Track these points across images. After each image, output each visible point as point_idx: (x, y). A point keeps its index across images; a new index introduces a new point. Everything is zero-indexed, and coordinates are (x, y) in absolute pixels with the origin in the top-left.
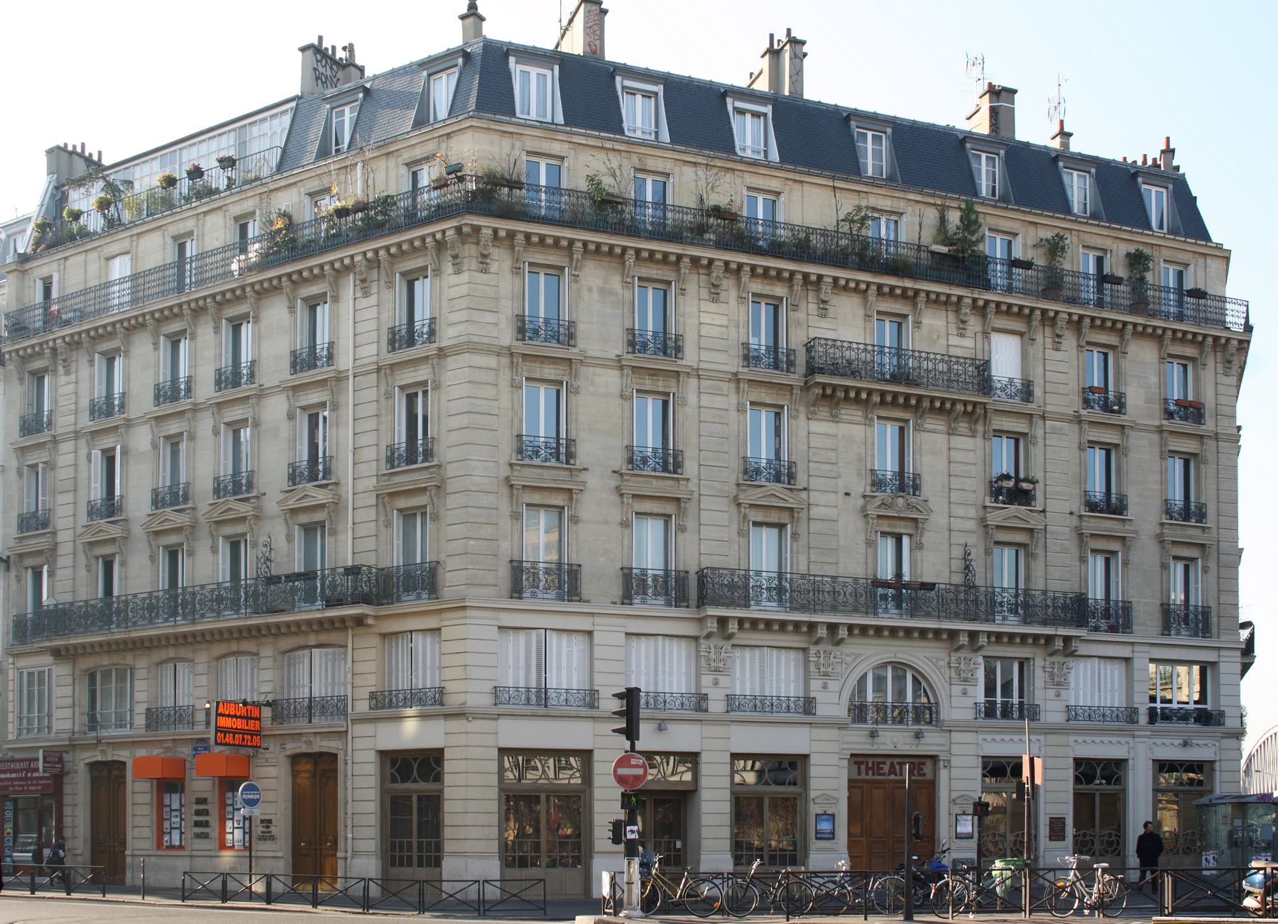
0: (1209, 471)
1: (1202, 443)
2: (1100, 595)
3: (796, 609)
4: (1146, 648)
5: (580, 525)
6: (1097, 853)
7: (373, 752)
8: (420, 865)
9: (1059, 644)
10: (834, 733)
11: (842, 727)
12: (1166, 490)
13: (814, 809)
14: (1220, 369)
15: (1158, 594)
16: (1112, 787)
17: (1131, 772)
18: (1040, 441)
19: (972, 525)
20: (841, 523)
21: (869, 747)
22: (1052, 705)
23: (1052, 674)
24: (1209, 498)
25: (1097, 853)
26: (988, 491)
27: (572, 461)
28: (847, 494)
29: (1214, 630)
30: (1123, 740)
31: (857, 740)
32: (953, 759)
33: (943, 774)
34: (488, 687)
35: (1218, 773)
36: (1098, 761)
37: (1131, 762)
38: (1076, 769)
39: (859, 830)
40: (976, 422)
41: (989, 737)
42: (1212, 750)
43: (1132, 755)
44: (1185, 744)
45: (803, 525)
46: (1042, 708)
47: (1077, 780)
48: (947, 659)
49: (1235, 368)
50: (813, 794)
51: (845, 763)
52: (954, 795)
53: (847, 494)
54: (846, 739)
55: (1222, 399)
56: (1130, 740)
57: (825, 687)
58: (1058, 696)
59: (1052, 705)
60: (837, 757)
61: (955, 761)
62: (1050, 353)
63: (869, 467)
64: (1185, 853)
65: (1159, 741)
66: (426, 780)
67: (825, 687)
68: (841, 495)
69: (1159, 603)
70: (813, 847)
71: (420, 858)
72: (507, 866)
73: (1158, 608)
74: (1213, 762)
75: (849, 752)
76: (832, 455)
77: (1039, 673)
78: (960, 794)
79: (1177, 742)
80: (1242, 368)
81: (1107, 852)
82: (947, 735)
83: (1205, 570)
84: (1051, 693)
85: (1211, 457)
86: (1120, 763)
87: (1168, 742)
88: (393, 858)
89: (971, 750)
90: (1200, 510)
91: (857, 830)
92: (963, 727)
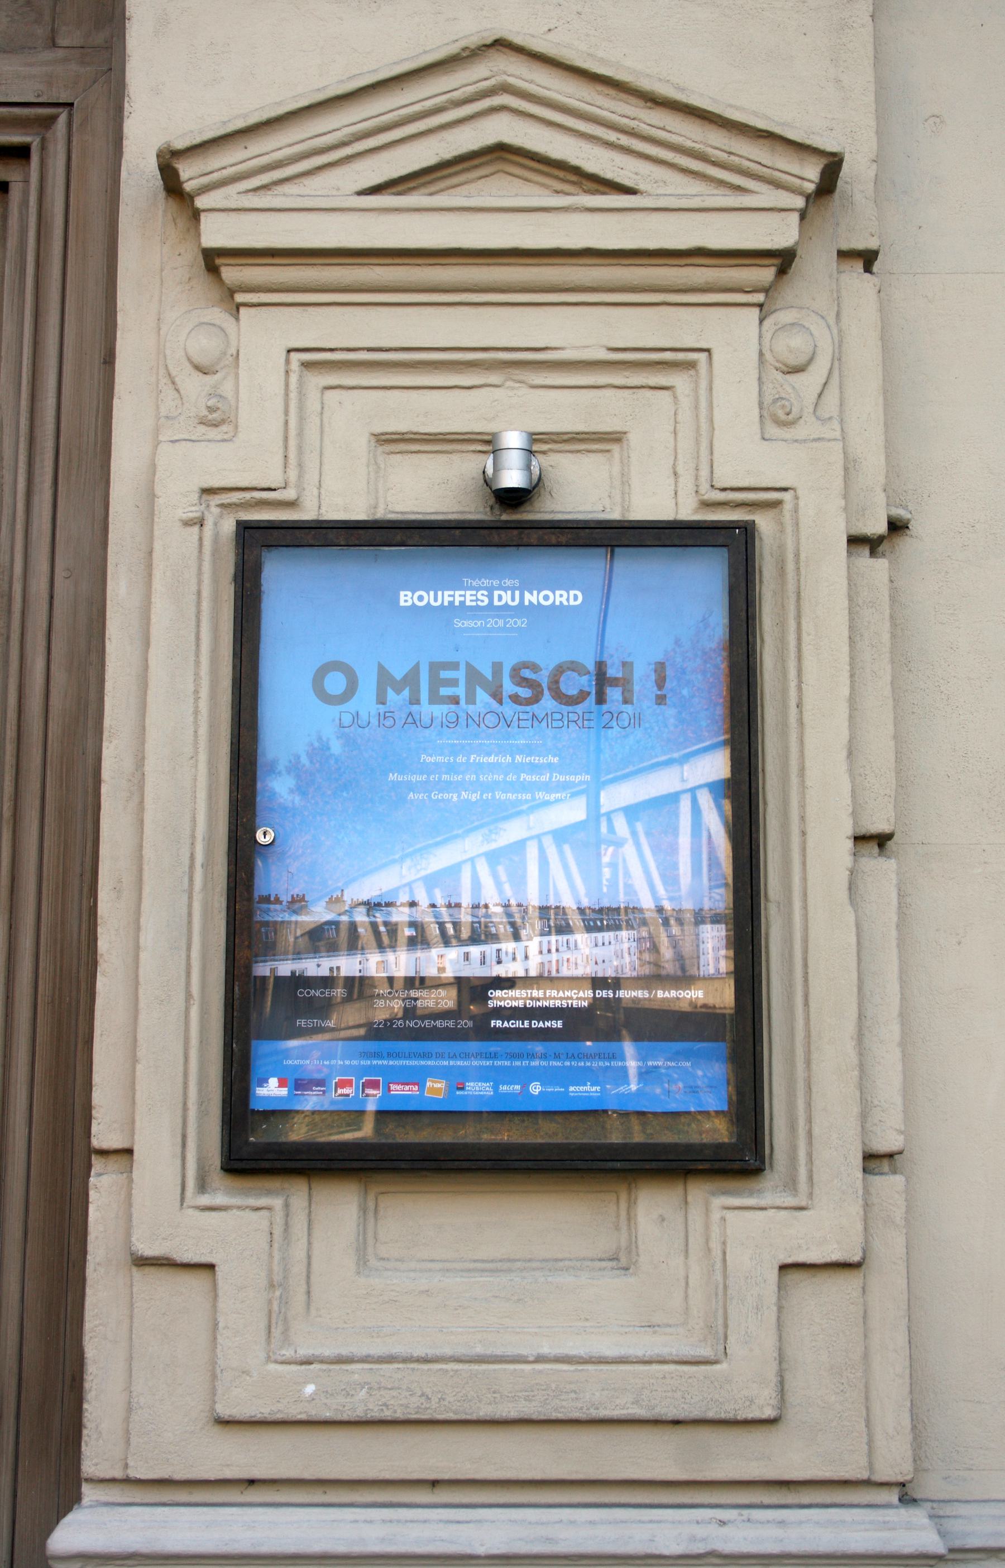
13: (213, 412)
70: (145, 1373)
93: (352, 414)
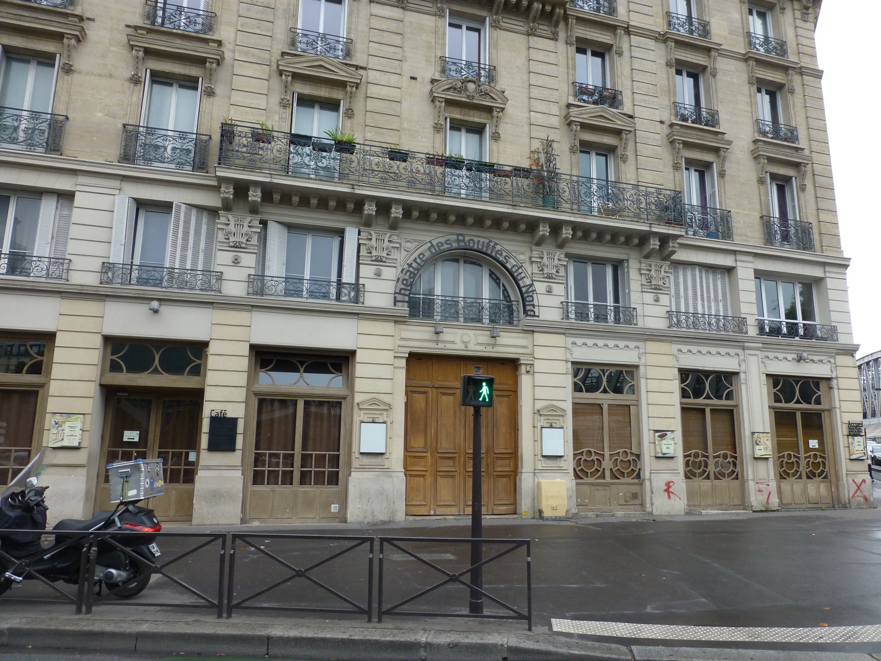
0: (796, 100)
1: (787, 75)
2: (695, 201)
3: (51, 150)
4: (750, 259)
5: (75, 76)
6: (712, 476)
7: (676, 371)
8: (303, 482)
9: (654, 244)
10: (388, 327)
11: (398, 320)
12: (757, 111)
14: (798, 14)
15: (758, 207)
16: (724, 402)
17: (743, 387)
18: (626, 54)
19: (555, 121)
20: (405, 104)
21: (433, 345)
22: (650, 310)
23: (650, 280)
24: (799, 121)
25: (712, 476)
26: (572, 92)
27: (492, 84)
28: (413, 78)
29: (817, 245)
30: (732, 351)
31: (419, 337)
32: (536, 362)
33: (525, 381)
34: (97, 264)
35: (836, 391)
36: (707, 373)
37: (742, 375)
38: (683, 381)
39: (422, 444)
40: (556, 25)
41: (579, 341)
42: (828, 366)
43: (743, 368)
44: (800, 359)
45: (809, 176)
46: (639, 312)
47: (684, 394)
48: (528, 255)
49: (811, 17)
50: (358, 398)
51: (403, 363)
52: (539, 405)
53: (413, 78)
54: (405, 334)
55: (802, 40)
56: (740, 351)
57: (378, 274)
58: (657, 300)
59: (230, 273)
60: (392, 354)
61: (539, 366)
62: (799, 23)
63: (439, 55)
64: (808, 477)
65: (771, 355)
66: (719, 397)
67: (378, 274)
68: (406, 78)
69: (758, 215)
71: (303, 474)
72: (782, 478)
73: (757, 221)
74: (829, 379)
75: (408, 350)
76: (397, 40)
77: (634, 275)
78: (546, 403)
79: (790, 357)
80: (816, 18)
81: (723, 475)
82: (529, 336)
83: (803, 188)
84: (649, 297)
85: (798, 89)
86: (730, 376)
87: (781, 356)
88: (256, 474)
89: (560, 354)
90: (713, 116)
91: (418, 442)
92: (550, 329)
93: (367, 416)
